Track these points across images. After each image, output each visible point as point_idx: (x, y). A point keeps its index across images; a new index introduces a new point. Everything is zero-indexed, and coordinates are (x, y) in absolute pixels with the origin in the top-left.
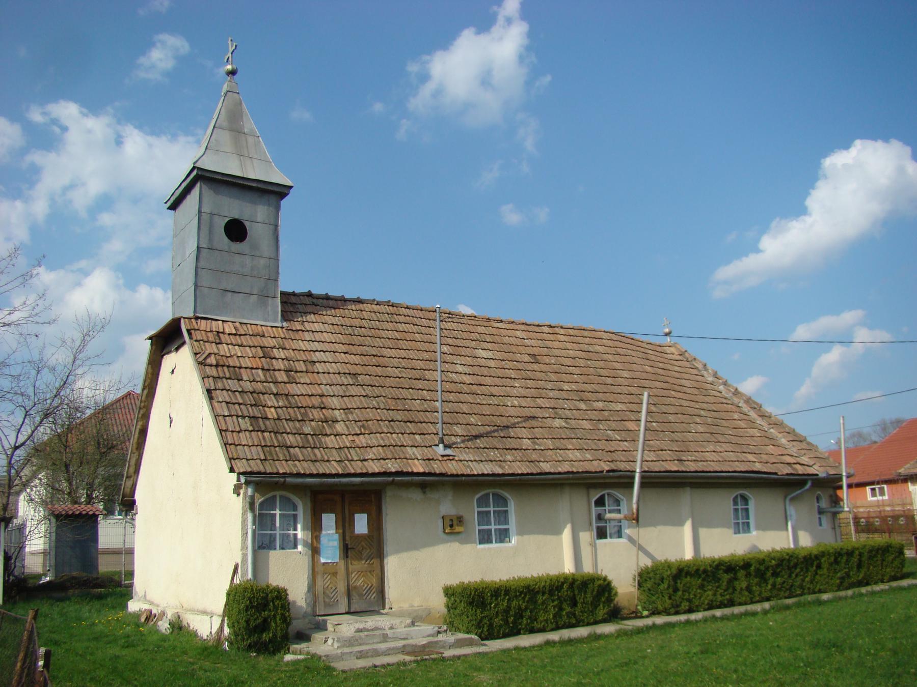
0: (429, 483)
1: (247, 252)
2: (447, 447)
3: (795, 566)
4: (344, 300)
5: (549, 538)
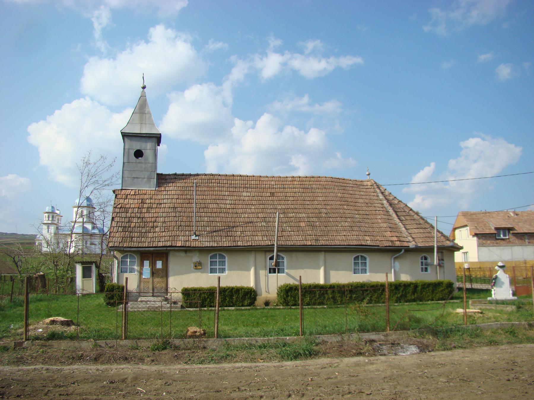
0: (187, 250)
1: (143, 162)
2: (196, 236)
3: (367, 290)
4: (190, 175)
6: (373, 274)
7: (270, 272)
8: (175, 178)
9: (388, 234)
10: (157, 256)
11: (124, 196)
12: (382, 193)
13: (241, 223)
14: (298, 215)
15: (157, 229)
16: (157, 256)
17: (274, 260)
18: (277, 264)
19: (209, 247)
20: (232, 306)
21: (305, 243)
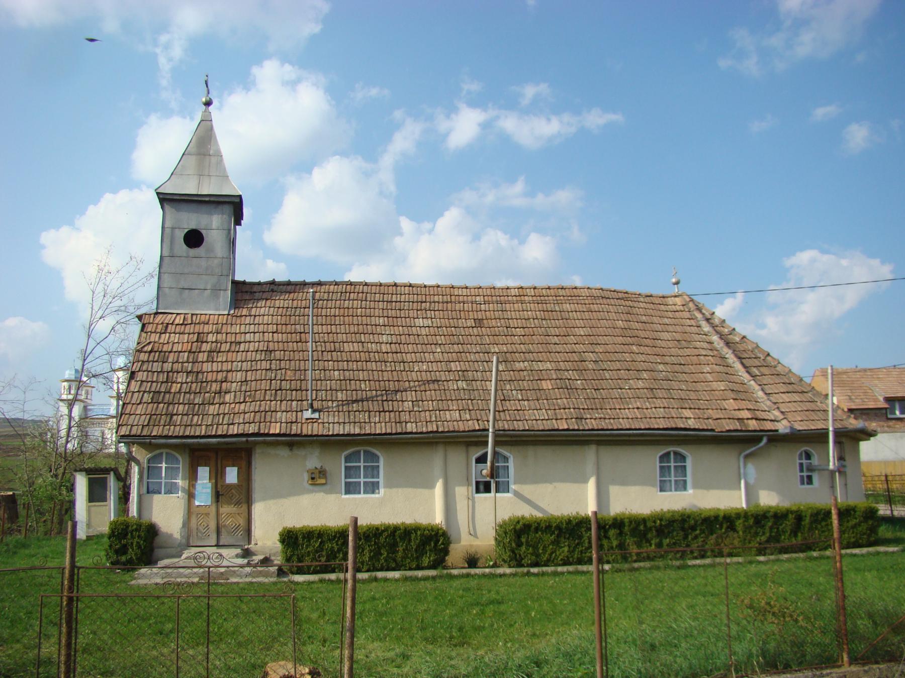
0: (293, 442)
1: (203, 255)
2: (314, 411)
3: (693, 528)
4: (304, 284)
5: (575, 486)
6: (700, 492)
7: (478, 491)
8: (273, 291)
9: (730, 404)
10: (227, 456)
11: (160, 327)
12: (708, 320)
13: (412, 384)
14: (535, 366)
15: (228, 398)
16: (227, 456)
17: (489, 463)
18: (494, 473)
19: (343, 435)
20: (394, 569)
21: (555, 425)
